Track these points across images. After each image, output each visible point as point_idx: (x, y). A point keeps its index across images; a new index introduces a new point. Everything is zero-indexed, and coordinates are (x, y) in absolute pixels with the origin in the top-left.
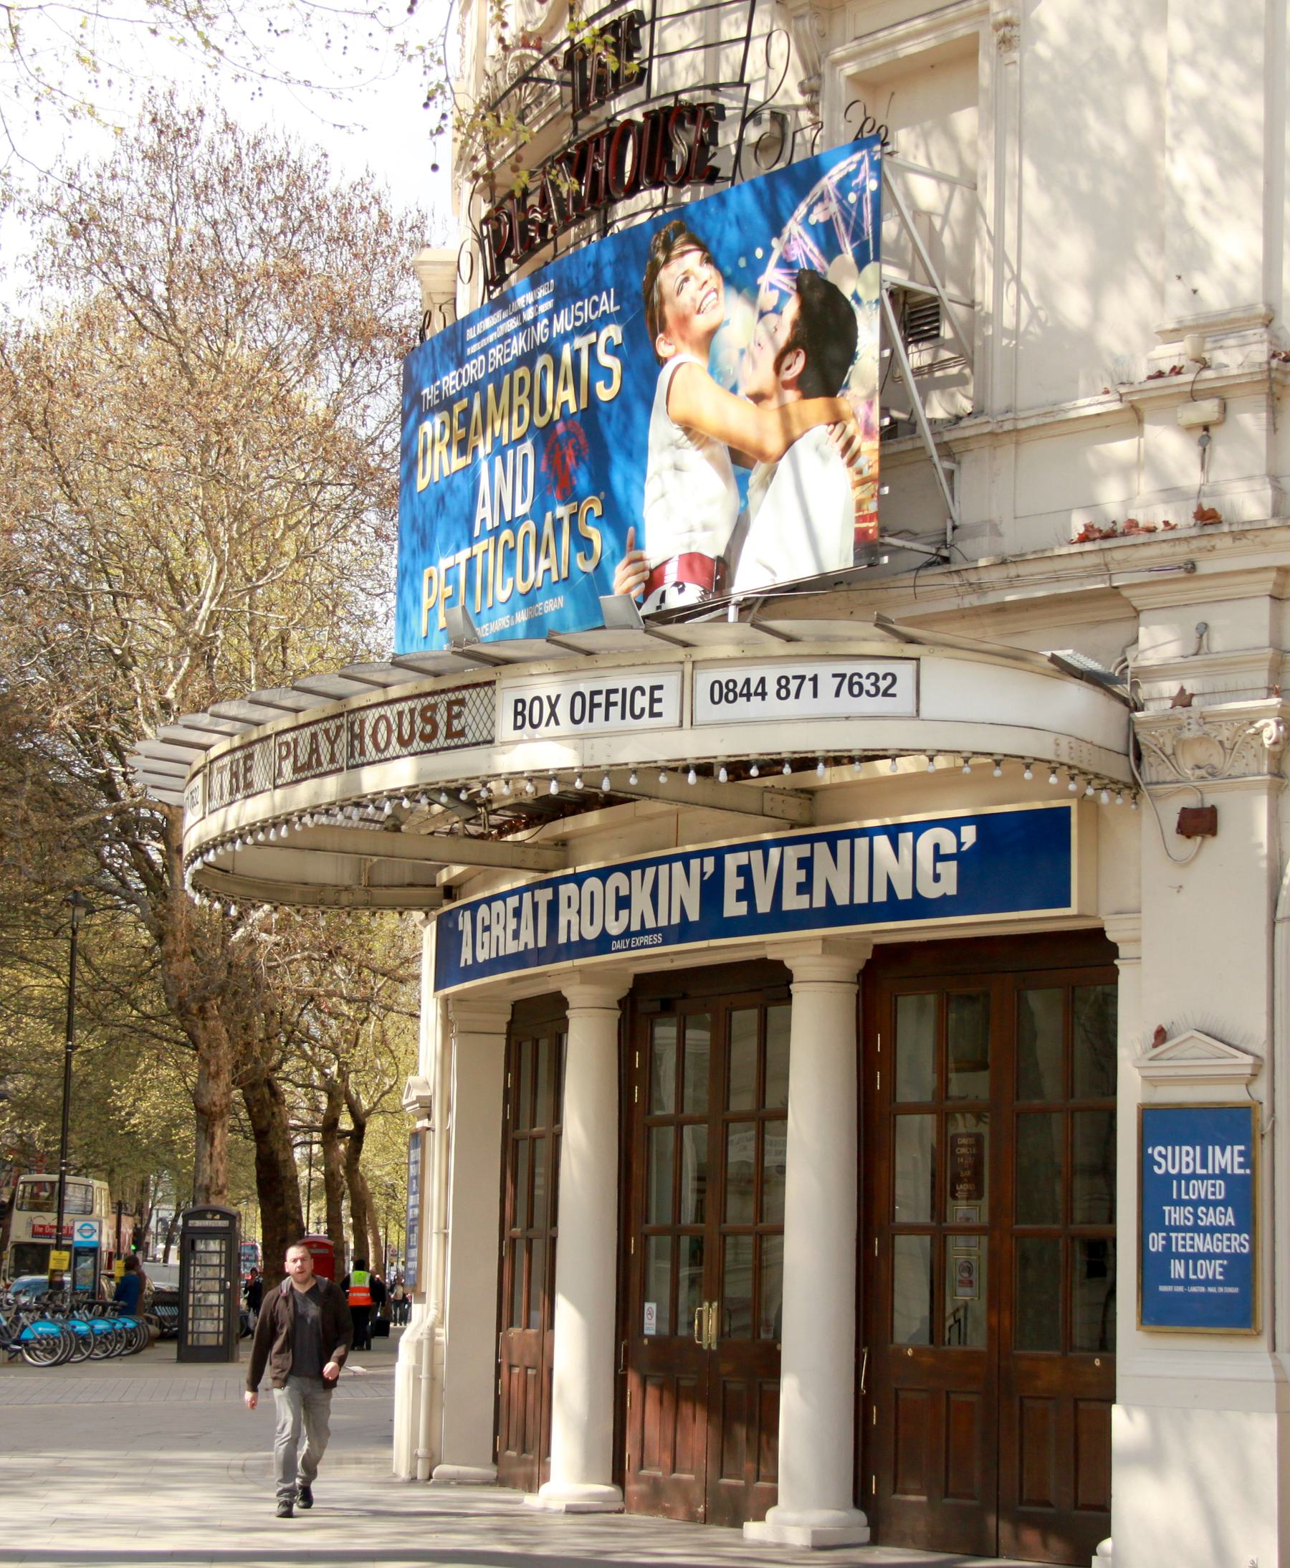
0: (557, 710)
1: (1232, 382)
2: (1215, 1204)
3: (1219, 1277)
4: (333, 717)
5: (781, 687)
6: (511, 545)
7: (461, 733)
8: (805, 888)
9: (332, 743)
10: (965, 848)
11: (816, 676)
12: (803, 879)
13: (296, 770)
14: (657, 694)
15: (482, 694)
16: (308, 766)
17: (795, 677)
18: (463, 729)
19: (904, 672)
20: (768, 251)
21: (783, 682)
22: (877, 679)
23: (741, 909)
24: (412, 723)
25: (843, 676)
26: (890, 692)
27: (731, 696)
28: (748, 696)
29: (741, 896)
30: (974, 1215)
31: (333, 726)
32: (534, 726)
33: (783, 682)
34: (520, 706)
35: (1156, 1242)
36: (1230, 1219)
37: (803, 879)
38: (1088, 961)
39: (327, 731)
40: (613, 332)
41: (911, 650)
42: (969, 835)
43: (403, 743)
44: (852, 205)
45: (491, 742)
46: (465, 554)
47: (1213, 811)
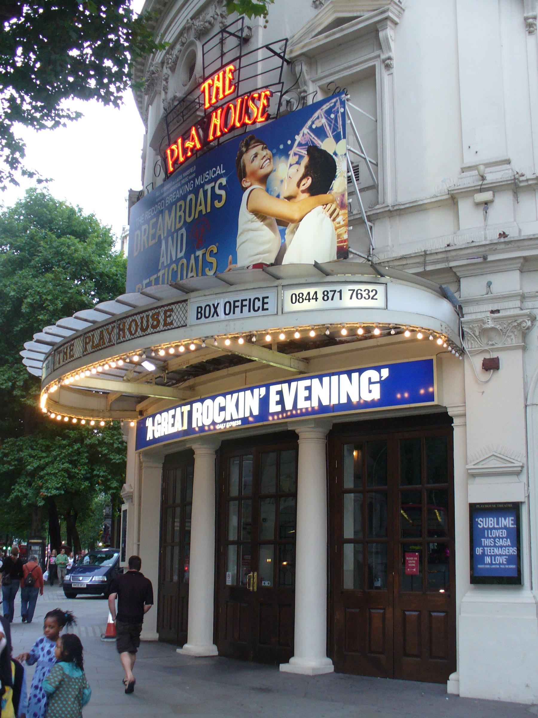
1: (498, 184)
4: (110, 323)
5: (325, 295)
6: (175, 269)
8: (308, 398)
9: (110, 334)
10: (382, 379)
11: (341, 290)
13: (93, 347)
14: (266, 300)
15: (181, 306)
16: (98, 345)
17: (331, 291)
18: (172, 321)
19: (380, 289)
20: (293, 141)
21: (326, 293)
22: (369, 292)
23: (279, 408)
24: (148, 321)
25: (354, 290)
26: (374, 298)
27: (301, 300)
28: (309, 300)
29: (278, 403)
31: (110, 327)
32: (206, 317)
33: (326, 293)
34: (200, 309)
36: (509, 543)
37: (307, 395)
38: (439, 426)
39: (107, 329)
40: (224, 181)
42: (385, 373)
43: (143, 330)
44: (332, 119)
45: (186, 326)
46: (155, 276)
47: (497, 359)
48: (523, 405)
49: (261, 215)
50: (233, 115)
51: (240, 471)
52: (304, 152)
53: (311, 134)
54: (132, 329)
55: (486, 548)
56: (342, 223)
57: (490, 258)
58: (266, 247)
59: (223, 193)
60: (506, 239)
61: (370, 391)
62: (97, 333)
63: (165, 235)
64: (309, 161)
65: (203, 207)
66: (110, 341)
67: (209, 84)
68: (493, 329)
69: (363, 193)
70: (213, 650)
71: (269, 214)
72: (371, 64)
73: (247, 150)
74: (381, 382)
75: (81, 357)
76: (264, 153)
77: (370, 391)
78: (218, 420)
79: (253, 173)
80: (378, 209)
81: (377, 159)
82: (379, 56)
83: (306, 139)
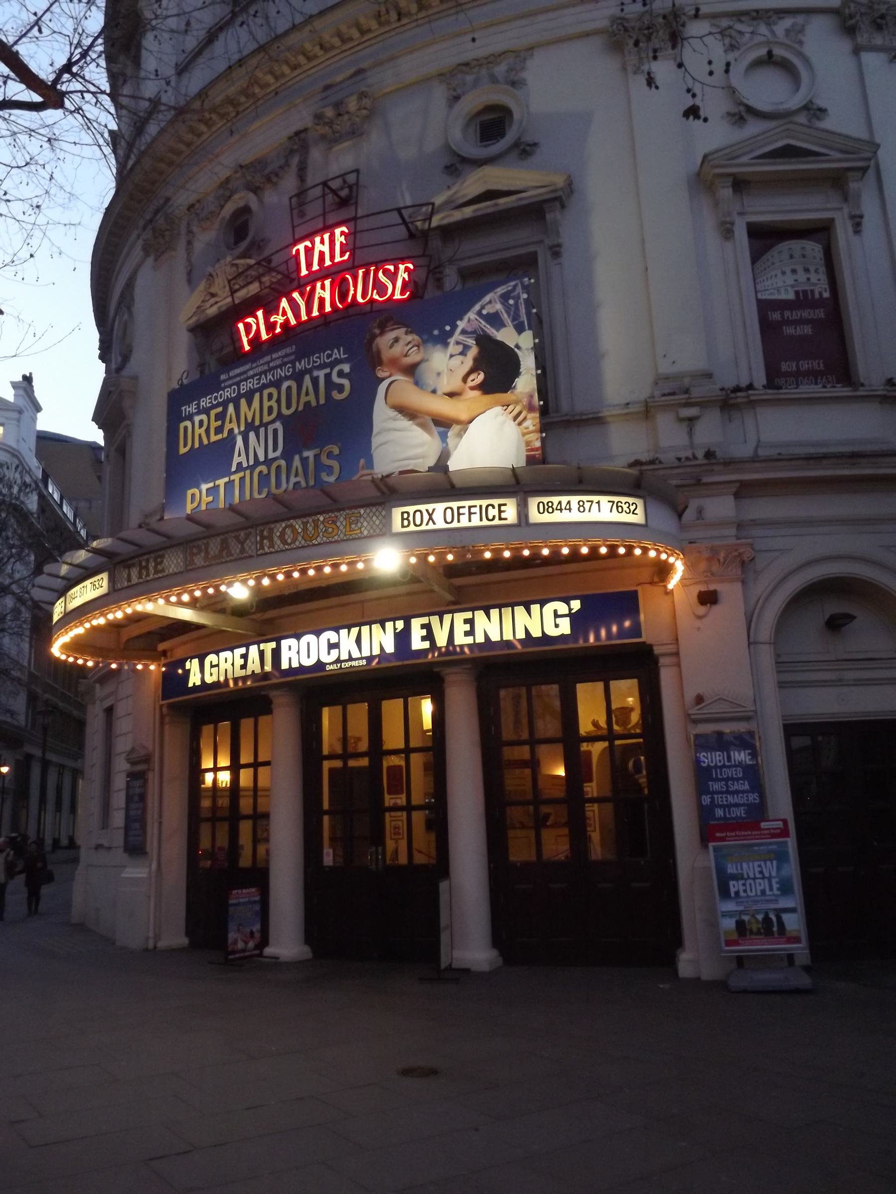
0: (434, 517)
2: (738, 779)
3: (743, 815)
8: (470, 633)
10: (573, 611)
12: (468, 629)
14: (503, 508)
20: (454, 327)
23: (426, 645)
28: (561, 510)
29: (424, 639)
30: (399, 802)
34: (405, 516)
35: (706, 800)
36: (747, 787)
37: (468, 629)
42: (576, 605)
49: (410, 413)
50: (352, 289)
51: (833, 681)
52: (471, 342)
53: (481, 321)
54: (286, 537)
55: (716, 796)
56: (532, 428)
57: (706, 480)
58: (418, 451)
59: (346, 382)
61: (557, 626)
63: (242, 428)
64: (480, 353)
65: (312, 398)
66: (243, 550)
67: (306, 247)
70: (184, 941)
71: (421, 412)
72: (531, 249)
73: (382, 333)
74: (570, 615)
75: (182, 572)
76: (410, 338)
77: (557, 626)
78: (325, 659)
79: (394, 363)
83: (474, 326)
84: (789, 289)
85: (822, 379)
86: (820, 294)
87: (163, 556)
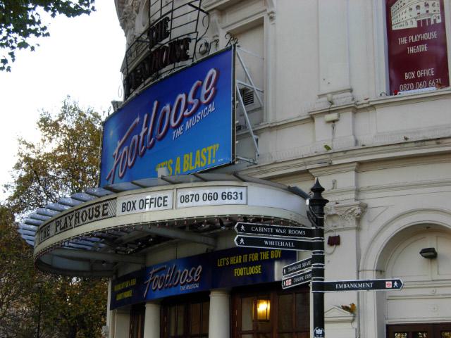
7: (107, 214)
13: (61, 229)
14: (166, 199)
16: (64, 228)
19: (243, 190)
32: (128, 211)
41: (245, 184)
43: (90, 218)
47: (339, 237)
48: (355, 271)
57: (335, 162)
60: (330, 151)
62: (63, 219)
66: (71, 225)
68: (335, 215)
69: (252, 114)
80: (262, 126)
81: (263, 88)
82: (266, 10)
84: (414, 20)
85: (432, 82)
86: (435, 20)
87: (107, 205)
